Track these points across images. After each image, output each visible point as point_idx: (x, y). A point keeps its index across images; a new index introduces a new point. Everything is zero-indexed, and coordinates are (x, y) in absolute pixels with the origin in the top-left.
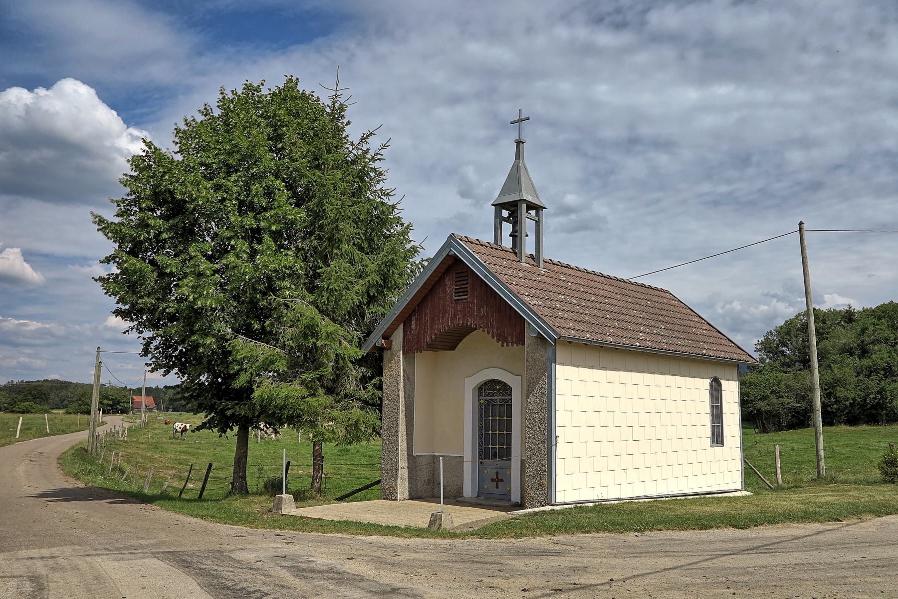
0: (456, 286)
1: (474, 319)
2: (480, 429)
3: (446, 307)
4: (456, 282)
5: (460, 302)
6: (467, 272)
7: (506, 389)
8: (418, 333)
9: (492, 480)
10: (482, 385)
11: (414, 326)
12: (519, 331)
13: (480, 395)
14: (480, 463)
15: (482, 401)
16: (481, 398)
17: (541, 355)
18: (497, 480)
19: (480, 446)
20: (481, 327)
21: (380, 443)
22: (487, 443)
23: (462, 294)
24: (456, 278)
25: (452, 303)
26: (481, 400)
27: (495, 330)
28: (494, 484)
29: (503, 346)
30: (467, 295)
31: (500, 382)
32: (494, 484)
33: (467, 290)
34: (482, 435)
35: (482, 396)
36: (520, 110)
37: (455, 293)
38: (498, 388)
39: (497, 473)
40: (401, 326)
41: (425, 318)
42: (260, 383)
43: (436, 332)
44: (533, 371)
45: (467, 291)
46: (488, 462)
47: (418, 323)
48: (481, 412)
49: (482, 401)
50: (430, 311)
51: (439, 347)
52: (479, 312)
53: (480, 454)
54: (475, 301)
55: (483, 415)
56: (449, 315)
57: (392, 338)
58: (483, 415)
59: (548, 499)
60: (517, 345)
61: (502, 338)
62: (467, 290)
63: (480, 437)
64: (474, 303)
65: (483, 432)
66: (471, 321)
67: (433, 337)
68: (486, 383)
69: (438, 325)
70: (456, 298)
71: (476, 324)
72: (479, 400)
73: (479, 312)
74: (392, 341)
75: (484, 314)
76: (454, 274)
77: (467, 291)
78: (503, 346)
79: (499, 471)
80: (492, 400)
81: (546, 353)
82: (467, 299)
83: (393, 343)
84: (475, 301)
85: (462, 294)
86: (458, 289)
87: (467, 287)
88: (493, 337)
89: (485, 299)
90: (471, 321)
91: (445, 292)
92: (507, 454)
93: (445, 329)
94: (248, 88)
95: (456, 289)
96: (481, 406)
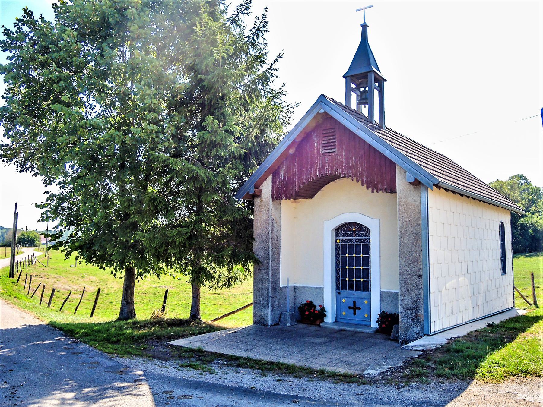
0: (323, 141)
1: (342, 169)
2: (337, 264)
4: (323, 137)
5: (328, 154)
6: (335, 128)
7: (363, 230)
8: (287, 183)
9: (350, 308)
10: (339, 228)
11: (282, 177)
13: (337, 235)
14: (338, 294)
15: (338, 241)
16: (337, 238)
17: (415, 200)
18: (355, 308)
19: (337, 279)
20: (350, 176)
22: (344, 276)
23: (329, 148)
24: (323, 134)
25: (320, 156)
26: (337, 240)
27: (365, 179)
29: (373, 192)
30: (335, 148)
31: (356, 224)
33: (334, 144)
34: (339, 270)
35: (338, 236)
36: (16, 204)
38: (354, 229)
39: (354, 302)
40: (270, 177)
41: (293, 170)
42: (115, 276)
43: (304, 181)
44: (405, 214)
45: (335, 145)
46: (344, 292)
48: (337, 250)
50: (298, 164)
51: (303, 195)
53: (337, 286)
54: (344, 154)
57: (261, 188)
59: (425, 333)
60: (377, 192)
61: (372, 185)
62: (334, 144)
63: (337, 271)
64: (343, 155)
65: (340, 267)
66: (340, 171)
67: (302, 186)
68: (342, 226)
69: (306, 175)
72: (336, 240)
74: (262, 190)
75: (352, 165)
76: (321, 131)
77: (335, 145)
78: (373, 192)
79: (356, 300)
80: (349, 240)
81: (419, 198)
82: (335, 152)
83: (263, 192)
84: (344, 154)
85: (329, 148)
86: (325, 143)
87: (335, 142)
88: (362, 185)
89: (354, 151)
90: (340, 171)
91: (313, 146)
92: (367, 287)
93: (313, 179)
94: (135, 221)
95: (323, 144)
96: (337, 245)
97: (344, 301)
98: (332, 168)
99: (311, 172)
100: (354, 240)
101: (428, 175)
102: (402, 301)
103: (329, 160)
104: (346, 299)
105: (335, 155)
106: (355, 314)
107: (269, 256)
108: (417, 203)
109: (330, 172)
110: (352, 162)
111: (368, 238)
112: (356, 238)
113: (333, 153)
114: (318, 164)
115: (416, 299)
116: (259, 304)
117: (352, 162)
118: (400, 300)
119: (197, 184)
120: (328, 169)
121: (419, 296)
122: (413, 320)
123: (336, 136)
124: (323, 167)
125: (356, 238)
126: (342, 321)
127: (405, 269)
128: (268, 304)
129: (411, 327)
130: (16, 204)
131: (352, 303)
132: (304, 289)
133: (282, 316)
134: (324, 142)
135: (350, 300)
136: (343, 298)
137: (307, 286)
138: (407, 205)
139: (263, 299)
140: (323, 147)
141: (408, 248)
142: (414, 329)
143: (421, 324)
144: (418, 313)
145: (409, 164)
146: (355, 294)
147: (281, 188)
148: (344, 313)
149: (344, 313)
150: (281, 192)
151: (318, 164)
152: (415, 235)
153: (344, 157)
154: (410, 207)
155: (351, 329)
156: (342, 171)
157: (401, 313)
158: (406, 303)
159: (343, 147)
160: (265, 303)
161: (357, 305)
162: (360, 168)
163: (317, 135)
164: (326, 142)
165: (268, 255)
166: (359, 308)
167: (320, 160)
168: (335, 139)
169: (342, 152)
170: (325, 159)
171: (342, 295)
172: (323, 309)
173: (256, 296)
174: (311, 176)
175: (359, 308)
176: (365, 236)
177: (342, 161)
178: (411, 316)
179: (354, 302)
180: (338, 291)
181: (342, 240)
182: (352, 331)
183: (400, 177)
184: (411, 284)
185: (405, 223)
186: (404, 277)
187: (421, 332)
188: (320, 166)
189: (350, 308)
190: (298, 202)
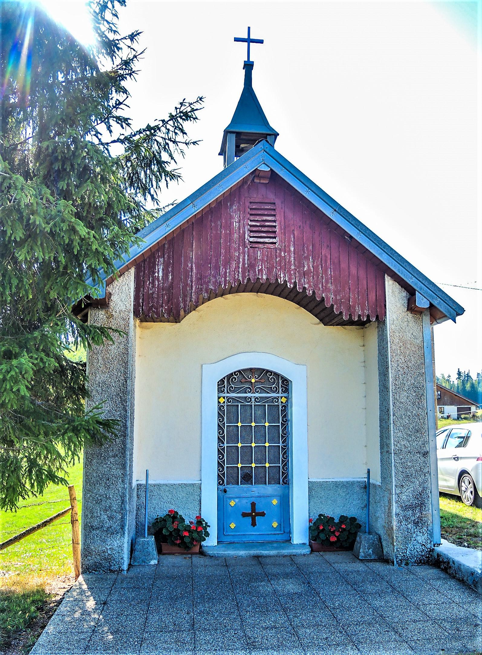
0: (251, 221)
1: (291, 275)
3: (232, 251)
4: (251, 215)
5: (261, 246)
11: (161, 274)
12: (374, 297)
13: (220, 390)
15: (222, 400)
16: (222, 395)
19: (220, 465)
21: (441, 483)
24: (251, 209)
25: (244, 246)
28: (249, 520)
30: (275, 238)
32: (249, 520)
33: (274, 229)
34: (223, 449)
35: (222, 392)
36: (249, 28)
37: (275, 232)
46: (233, 489)
47: (170, 269)
48: (220, 416)
49: (222, 400)
52: (300, 265)
54: (292, 249)
55: (225, 420)
56: (238, 263)
58: (225, 420)
62: (274, 229)
64: (290, 251)
65: (226, 445)
70: (251, 240)
71: (295, 282)
73: (300, 265)
76: (247, 204)
82: (275, 243)
84: (292, 249)
87: (275, 227)
91: (229, 226)
95: (251, 226)
96: (220, 408)
97: (232, 503)
98: (270, 271)
99: (226, 272)
100: (253, 399)
101: (448, 299)
102: (398, 495)
103: (263, 255)
104: (237, 500)
105: (276, 249)
106: (254, 524)
107: (127, 428)
108: (418, 342)
109: (265, 277)
110: (309, 266)
111: (278, 395)
112: (257, 395)
113: (272, 246)
114: (241, 260)
115: (420, 489)
116: (97, 529)
117: (309, 266)
118: (396, 493)
119: (49, 253)
120: (261, 271)
121: (425, 485)
122: (416, 524)
123: (278, 218)
124: (252, 266)
125: (257, 395)
126: (229, 539)
127: (402, 443)
128: (123, 527)
129: (414, 535)
130: (249, 28)
131: (249, 506)
132: (160, 490)
133: (138, 547)
134: (254, 223)
135: (244, 501)
136: (231, 498)
137: (162, 482)
138: (404, 343)
139: (110, 518)
140: (251, 231)
141: (406, 410)
142: (419, 538)
143: (429, 528)
144: (424, 513)
145: (421, 279)
146: (254, 489)
147: (158, 295)
148: (233, 526)
149: (233, 526)
150: (158, 302)
151: (241, 260)
152: (417, 391)
153: (292, 255)
154: (409, 346)
155: (273, 552)
156: (290, 279)
157: (398, 515)
158: (404, 497)
159: (290, 238)
160: (116, 526)
161: (259, 508)
162: (322, 277)
163: (239, 210)
164: (258, 224)
165: (234, 426)
166: (263, 514)
167: (244, 253)
168: (275, 221)
169: (289, 246)
170: (255, 254)
171: (228, 495)
172: (200, 521)
173: (92, 512)
174: (225, 280)
175: (263, 514)
176: (274, 392)
177: (290, 262)
178: (413, 518)
179: (253, 505)
180: (221, 487)
181: (229, 399)
182: (273, 556)
183: (392, 299)
184: (413, 466)
185: (402, 372)
186: (401, 457)
187: (429, 541)
188: (244, 264)
189: (244, 515)
190: (146, 328)
